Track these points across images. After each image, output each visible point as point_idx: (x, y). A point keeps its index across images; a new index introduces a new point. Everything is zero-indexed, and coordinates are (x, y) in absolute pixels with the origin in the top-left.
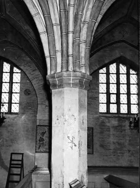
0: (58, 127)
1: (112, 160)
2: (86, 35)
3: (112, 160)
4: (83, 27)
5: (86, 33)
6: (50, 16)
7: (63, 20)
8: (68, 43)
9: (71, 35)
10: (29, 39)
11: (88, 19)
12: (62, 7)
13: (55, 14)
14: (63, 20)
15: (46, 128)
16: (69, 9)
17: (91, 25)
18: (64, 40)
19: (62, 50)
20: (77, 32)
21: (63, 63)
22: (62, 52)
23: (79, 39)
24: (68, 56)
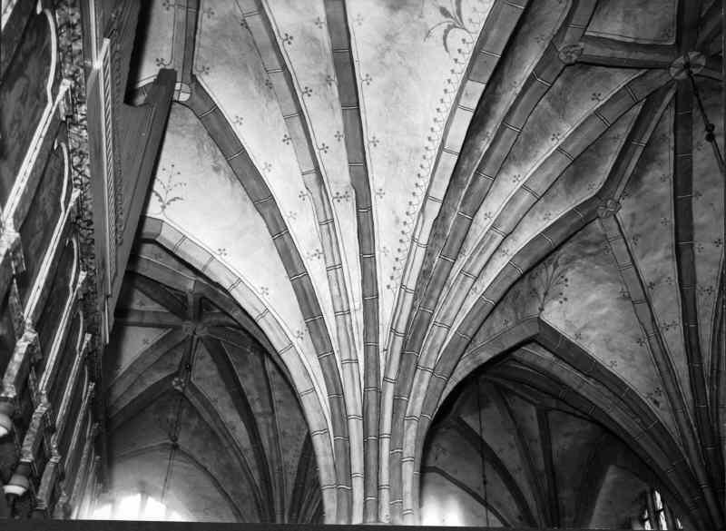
0: (429, 32)
1: (173, 435)
2: (413, 445)
3: (173, 435)
4: (408, 427)
5: (413, 439)
6: (352, 489)
7: (373, 409)
8: (378, 458)
9: (386, 443)
10: (262, 316)
11: (417, 412)
12: (372, 383)
13: (354, 395)
14: (373, 409)
15: (660, 255)
16: (385, 386)
17: (436, 388)
18: (372, 453)
19: (365, 473)
20: (396, 436)
21: (368, 503)
22: (365, 478)
23: (401, 453)
24: (379, 488)
